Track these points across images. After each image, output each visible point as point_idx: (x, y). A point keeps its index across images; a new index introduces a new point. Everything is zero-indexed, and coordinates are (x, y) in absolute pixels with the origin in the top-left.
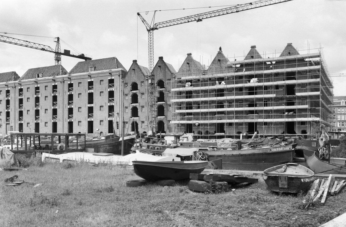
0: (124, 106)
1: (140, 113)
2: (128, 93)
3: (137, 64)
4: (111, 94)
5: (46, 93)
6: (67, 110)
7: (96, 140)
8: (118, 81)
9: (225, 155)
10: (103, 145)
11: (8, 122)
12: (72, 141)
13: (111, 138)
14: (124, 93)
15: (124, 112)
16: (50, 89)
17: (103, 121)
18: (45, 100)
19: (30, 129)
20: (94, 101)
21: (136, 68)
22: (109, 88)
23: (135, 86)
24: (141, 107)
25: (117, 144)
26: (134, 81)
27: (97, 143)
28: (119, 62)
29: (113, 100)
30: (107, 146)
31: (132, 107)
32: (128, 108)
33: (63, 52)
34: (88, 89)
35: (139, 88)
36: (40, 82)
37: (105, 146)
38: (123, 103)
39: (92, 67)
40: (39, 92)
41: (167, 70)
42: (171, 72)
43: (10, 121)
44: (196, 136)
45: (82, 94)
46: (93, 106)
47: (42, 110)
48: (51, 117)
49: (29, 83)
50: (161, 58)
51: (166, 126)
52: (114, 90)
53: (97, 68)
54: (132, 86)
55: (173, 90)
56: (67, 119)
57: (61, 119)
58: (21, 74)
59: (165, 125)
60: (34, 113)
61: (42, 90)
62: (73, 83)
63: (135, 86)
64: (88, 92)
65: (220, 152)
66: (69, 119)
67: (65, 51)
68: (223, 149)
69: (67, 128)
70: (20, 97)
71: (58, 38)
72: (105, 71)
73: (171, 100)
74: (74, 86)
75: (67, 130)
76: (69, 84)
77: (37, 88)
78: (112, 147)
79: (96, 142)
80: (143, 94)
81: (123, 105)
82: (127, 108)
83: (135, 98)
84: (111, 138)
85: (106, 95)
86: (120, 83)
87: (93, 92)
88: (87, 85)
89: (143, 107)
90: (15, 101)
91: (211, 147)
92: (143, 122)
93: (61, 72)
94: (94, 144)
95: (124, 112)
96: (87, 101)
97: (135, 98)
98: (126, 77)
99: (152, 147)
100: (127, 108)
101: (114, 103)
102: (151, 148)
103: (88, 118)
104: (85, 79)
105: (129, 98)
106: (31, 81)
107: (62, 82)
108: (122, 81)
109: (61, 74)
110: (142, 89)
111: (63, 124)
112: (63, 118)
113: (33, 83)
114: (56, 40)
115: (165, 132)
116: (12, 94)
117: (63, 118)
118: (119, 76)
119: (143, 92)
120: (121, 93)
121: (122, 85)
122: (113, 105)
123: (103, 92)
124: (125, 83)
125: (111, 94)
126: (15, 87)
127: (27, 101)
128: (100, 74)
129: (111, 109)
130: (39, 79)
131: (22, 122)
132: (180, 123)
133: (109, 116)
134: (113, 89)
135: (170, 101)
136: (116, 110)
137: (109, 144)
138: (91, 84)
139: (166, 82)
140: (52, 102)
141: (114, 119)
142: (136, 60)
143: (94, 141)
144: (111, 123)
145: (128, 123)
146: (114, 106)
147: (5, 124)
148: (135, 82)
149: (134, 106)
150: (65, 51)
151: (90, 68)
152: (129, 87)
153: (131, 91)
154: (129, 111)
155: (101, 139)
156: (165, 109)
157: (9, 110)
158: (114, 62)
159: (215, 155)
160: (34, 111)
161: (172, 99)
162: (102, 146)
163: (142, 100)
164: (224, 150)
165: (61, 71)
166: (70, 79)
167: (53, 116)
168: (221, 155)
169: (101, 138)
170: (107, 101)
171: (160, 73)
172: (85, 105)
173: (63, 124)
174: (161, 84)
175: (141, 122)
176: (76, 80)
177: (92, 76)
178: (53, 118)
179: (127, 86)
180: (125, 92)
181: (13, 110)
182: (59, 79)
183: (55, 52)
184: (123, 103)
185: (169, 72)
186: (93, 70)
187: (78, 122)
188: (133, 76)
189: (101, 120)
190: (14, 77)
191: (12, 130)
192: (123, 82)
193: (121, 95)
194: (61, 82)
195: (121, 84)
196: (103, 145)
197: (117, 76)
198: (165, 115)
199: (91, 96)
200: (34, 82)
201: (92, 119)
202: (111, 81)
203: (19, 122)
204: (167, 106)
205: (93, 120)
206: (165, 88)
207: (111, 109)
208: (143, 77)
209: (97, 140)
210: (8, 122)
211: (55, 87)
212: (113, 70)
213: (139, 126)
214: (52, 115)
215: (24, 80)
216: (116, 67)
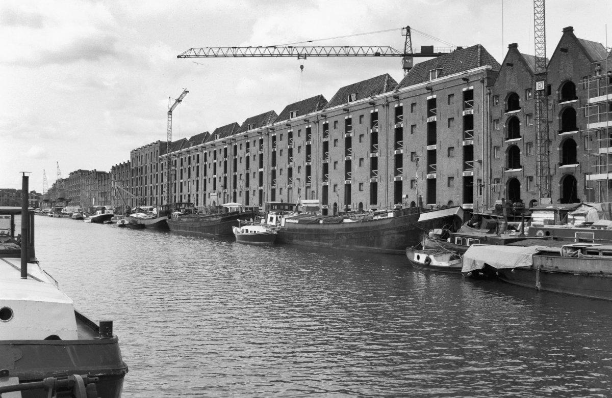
0: (493, 146)
1: (523, 159)
2: (500, 116)
3: (517, 52)
4: (468, 122)
5: (361, 128)
6: (393, 158)
7: (379, 220)
8: (481, 96)
9: (601, 273)
10: (388, 229)
11: (308, 185)
12: (342, 221)
13: (402, 216)
14: (491, 117)
15: (491, 157)
16: (367, 120)
17: (453, 178)
18: (360, 142)
19: (338, 195)
20: (437, 138)
21: (515, 61)
22: (464, 110)
23: (513, 101)
24: (525, 146)
25: (413, 228)
26: (510, 89)
27: (377, 227)
28: (487, 53)
29: (472, 133)
30: (394, 232)
31: (506, 147)
32: (501, 149)
33: (419, 51)
34: (426, 115)
35: (521, 105)
36: (355, 108)
37: (391, 231)
38: (491, 140)
39: (434, 71)
40: (350, 128)
41: (581, 56)
42: (590, 60)
43: (312, 182)
44: (511, 217)
45: (417, 126)
46: (435, 148)
47: (355, 160)
48: (369, 173)
49: (336, 113)
50: (568, 31)
51: (580, 186)
52: (472, 113)
53: (443, 72)
54: (509, 102)
55: (592, 100)
56: (393, 175)
57: (383, 177)
58: (329, 98)
59: (578, 184)
60: (344, 166)
61: (355, 124)
62: (402, 107)
63: (513, 101)
64: (428, 121)
65: (588, 262)
66: (395, 175)
67: (423, 48)
68: (604, 254)
69: (394, 194)
70: (325, 140)
71: (408, 29)
72: (455, 75)
73: (588, 125)
74: (404, 111)
75: (393, 196)
76: (396, 108)
77: (349, 121)
78: (403, 236)
79: (379, 223)
80: (529, 115)
81: (491, 145)
82: (497, 148)
83: (513, 128)
84: (402, 216)
85: (459, 124)
86: (485, 97)
87: (435, 120)
88: (425, 107)
89: (530, 144)
90: (318, 147)
91: (569, 248)
92: (531, 179)
93: (385, 87)
94: (374, 227)
95: (492, 158)
96: (426, 139)
97: (513, 128)
98: (497, 83)
99: (472, 239)
100: (497, 148)
101: (473, 141)
102: (459, 241)
103: (428, 173)
104: (422, 96)
105: (502, 126)
106: (338, 110)
107: (385, 107)
108: (488, 91)
109: (384, 90)
110: (527, 103)
111: (387, 186)
112: (387, 174)
113: (342, 112)
114: (405, 31)
115: (578, 201)
116: (313, 135)
117: (387, 174)
118: (483, 82)
119: (530, 112)
120: (485, 118)
121: (487, 102)
122: (472, 143)
123: (453, 118)
124: (494, 96)
125: (468, 122)
126: (318, 122)
127: (333, 146)
128: (448, 83)
129: (468, 152)
130: (351, 103)
131: (328, 184)
132: (610, 178)
133: (466, 167)
134: (471, 112)
135: (586, 128)
136: (479, 153)
137: (398, 229)
138: (432, 104)
139: (579, 84)
140: (370, 144)
141: (478, 172)
142: (517, 44)
143: (375, 220)
144: (468, 180)
145: (501, 180)
146: (474, 147)
147: (305, 187)
148: (514, 90)
149: (513, 143)
150: (423, 48)
151: (431, 73)
152: (503, 102)
153: (507, 111)
154: (502, 156)
155: (386, 217)
156: (578, 147)
157: (310, 163)
158: (479, 54)
159: (575, 270)
160: (344, 162)
161: (590, 123)
162: (386, 233)
163: (528, 129)
164: (605, 257)
165: (386, 85)
166: (398, 98)
167: (371, 171)
168: (591, 273)
169: (387, 215)
170: (460, 136)
171: (565, 66)
172: (421, 148)
173: (387, 186)
174: (568, 90)
175: (526, 179)
176: (407, 100)
177: (434, 88)
178: (371, 174)
179: (497, 101)
180: (493, 116)
181: (315, 162)
182: (380, 101)
183: (402, 55)
184: (491, 140)
185: (587, 60)
186: (436, 76)
187: (410, 182)
188: (510, 80)
189: (450, 176)
190: (319, 105)
191: (314, 199)
192: (490, 94)
193: (486, 122)
194: (383, 106)
195: (487, 97)
196: (388, 229)
197: (479, 84)
198: (578, 160)
199: (432, 127)
200: (342, 111)
201: (435, 176)
202: (469, 95)
203: (323, 184)
204: (583, 140)
205: (435, 177)
206: (576, 98)
207: (468, 152)
208: (530, 78)
209: (381, 219)
210: (308, 185)
211: (374, 116)
212: (470, 71)
213: (522, 187)
214: (370, 170)
215: (331, 109)
216: (479, 65)
